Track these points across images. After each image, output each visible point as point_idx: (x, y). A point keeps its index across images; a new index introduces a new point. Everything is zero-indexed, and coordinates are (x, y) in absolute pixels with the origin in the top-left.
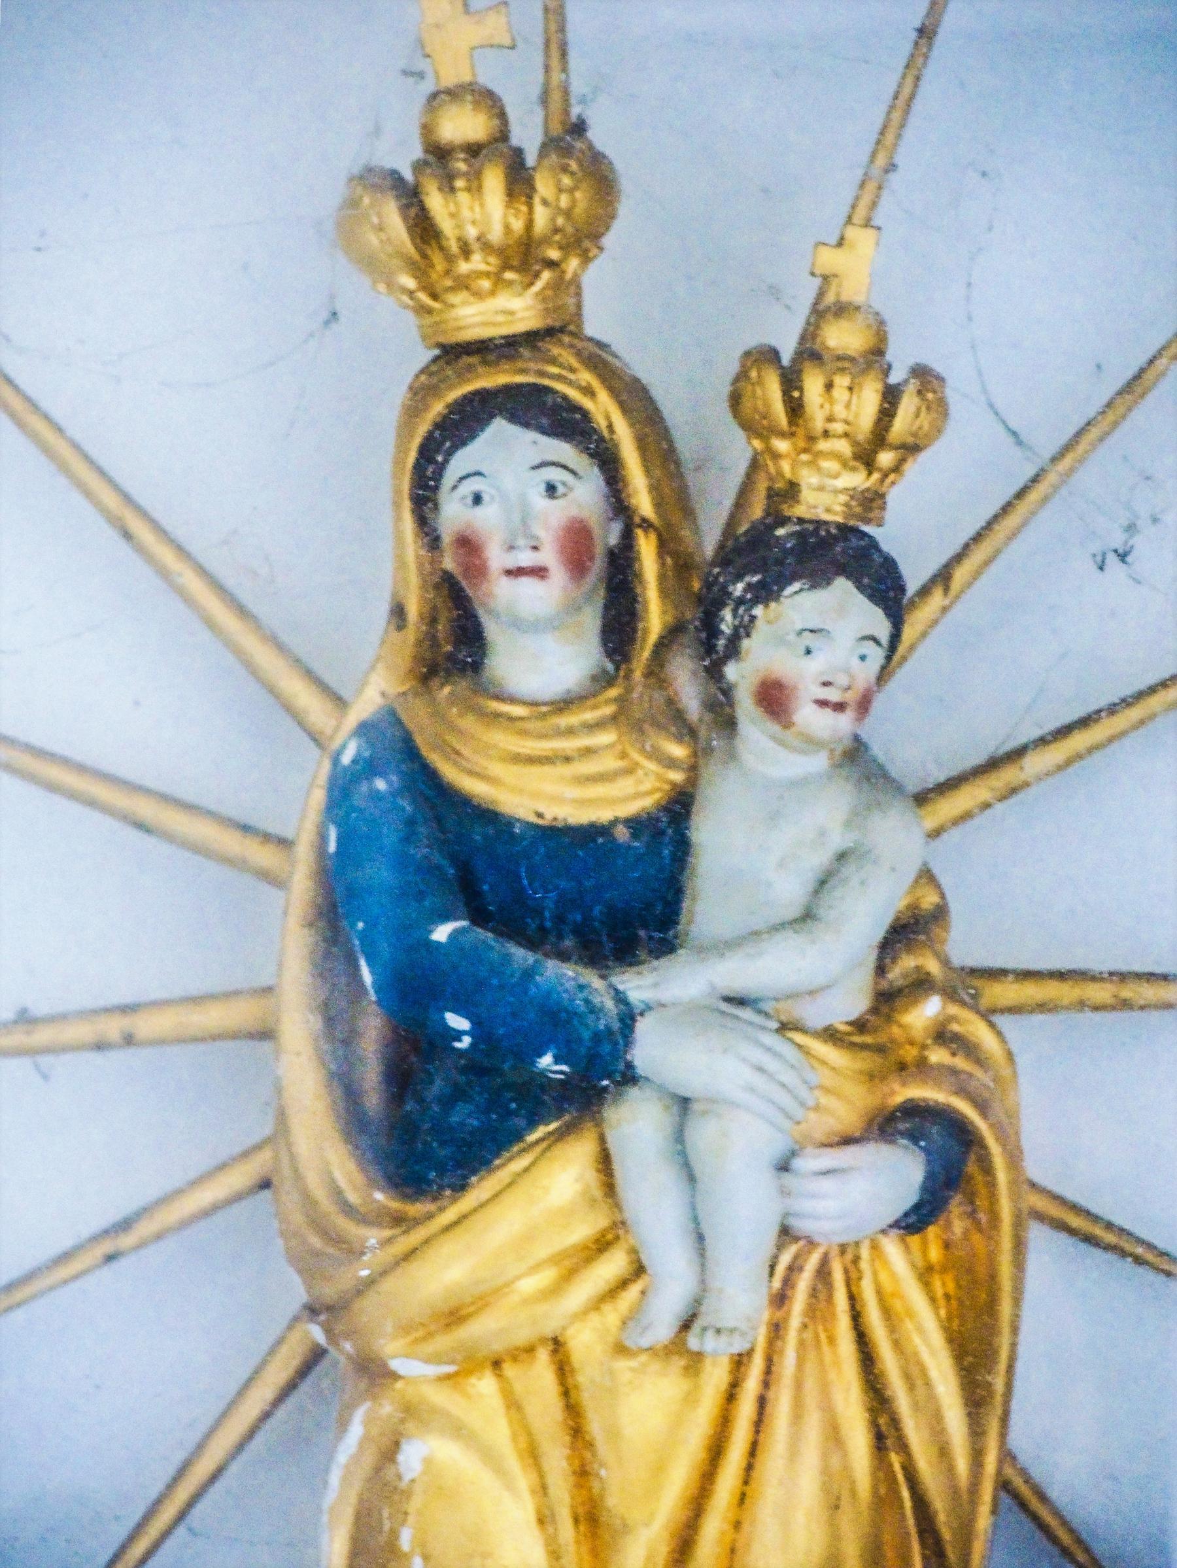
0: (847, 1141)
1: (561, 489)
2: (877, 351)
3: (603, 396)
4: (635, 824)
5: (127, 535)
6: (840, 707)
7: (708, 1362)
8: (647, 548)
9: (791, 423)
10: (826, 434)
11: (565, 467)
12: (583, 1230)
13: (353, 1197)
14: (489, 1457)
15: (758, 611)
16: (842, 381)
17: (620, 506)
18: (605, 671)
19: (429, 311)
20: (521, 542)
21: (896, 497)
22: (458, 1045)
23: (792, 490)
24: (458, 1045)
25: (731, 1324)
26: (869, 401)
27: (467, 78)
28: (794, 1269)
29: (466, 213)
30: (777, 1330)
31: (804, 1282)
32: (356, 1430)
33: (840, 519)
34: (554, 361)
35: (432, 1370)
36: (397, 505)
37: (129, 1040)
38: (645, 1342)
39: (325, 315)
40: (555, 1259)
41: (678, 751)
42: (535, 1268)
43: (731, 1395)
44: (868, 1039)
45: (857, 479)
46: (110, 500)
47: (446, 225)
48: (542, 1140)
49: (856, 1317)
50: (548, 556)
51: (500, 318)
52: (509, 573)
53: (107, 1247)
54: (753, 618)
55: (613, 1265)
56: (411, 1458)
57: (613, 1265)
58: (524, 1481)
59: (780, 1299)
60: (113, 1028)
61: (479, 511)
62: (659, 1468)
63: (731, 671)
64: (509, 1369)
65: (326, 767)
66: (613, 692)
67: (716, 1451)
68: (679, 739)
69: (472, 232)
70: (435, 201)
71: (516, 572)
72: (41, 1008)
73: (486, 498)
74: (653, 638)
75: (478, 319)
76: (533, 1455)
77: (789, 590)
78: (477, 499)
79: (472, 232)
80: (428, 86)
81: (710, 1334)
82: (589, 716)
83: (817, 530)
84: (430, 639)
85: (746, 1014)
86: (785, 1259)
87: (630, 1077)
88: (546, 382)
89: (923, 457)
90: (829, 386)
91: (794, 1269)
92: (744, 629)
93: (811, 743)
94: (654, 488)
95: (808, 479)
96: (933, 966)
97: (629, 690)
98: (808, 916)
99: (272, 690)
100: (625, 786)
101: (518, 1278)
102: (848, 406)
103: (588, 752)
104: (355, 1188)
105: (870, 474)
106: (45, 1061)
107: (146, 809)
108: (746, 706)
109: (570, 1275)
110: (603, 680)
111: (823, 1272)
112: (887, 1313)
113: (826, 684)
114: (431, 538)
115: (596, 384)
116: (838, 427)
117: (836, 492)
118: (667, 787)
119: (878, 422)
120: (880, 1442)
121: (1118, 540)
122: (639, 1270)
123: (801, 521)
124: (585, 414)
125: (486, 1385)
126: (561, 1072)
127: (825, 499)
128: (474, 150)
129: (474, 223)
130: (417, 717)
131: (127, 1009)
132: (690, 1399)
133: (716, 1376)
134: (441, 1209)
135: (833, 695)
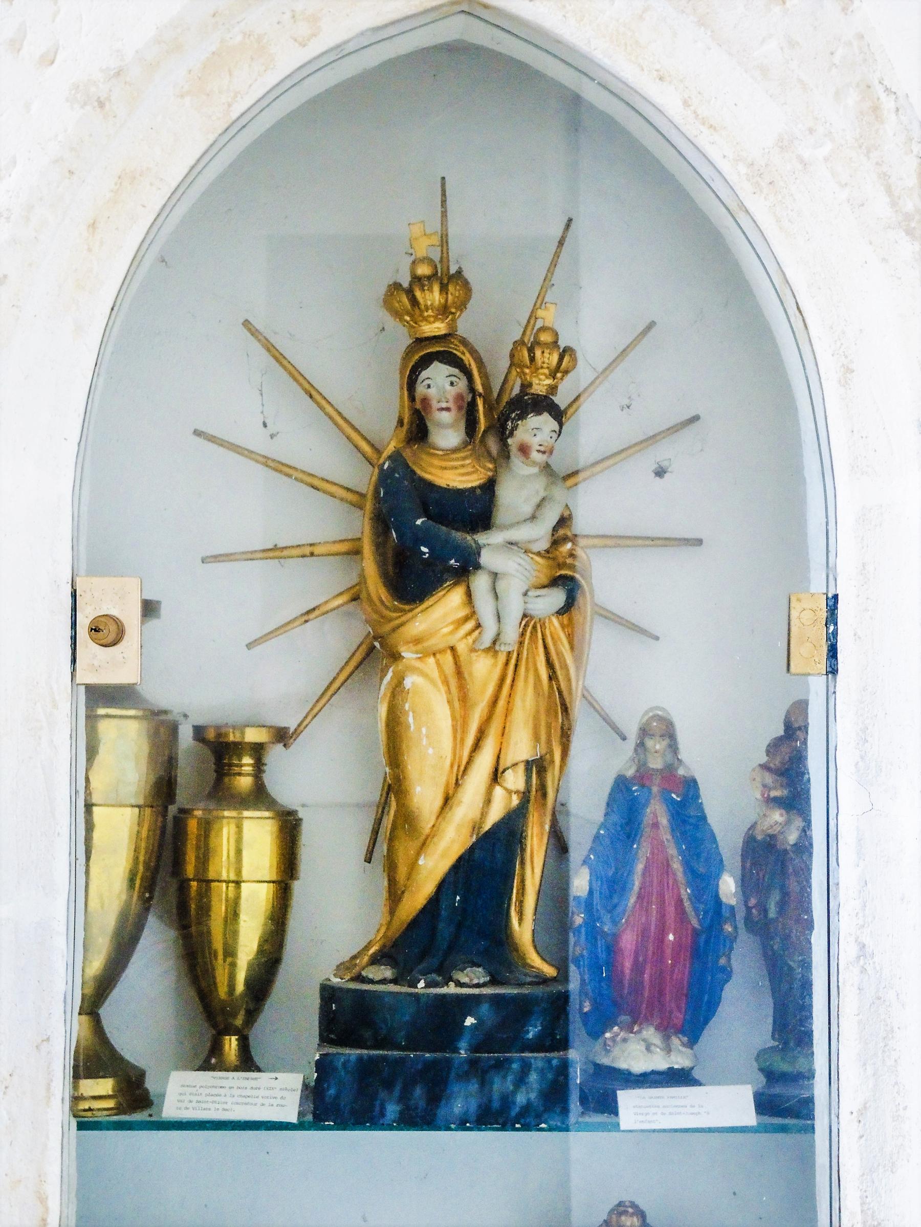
0: (544, 587)
1: (455, 384)
2: (555, 343)
3: (467, 355)
4: (480, 487)
5: (311, 396)
6: (544, 452)
7: (500, 653)
8: (480, 403)
9: (531, 364)
10: (542, 367)
11: (455, 376)
12: (462, 613)
13: (388, 604)
14: (432, 681)
15: (519, 422)
16: (547, 351)
17: (472, 389)
18: (467, 441)
19: (414, 327)
20: (443, 399)
21: (561, 388)
22: (424, 557)
23: (530, 385)
24: (424, 557)
25: (509, 642)
26: (555, 358)
27: (425, 255)
28: (526, 626)
29: (427, 297)
30: (521, 643)
31: (529, 629)
32: (390, 674)
33: (545, 394)
34: (452, 343)
35: (415, 656)
36: (402, 388)
37: (312, 554)
38: (482, 647)
39: (381, 328)
40: (452, 623)
41: (491, 466)
42: (447, 626)
43: (507, 663)
44: (551, 556)
45: (549, 382)
46: (307, 386)
47: (421, 300)
48: (449, 586)
49: (544, 640)
50: (451, 405)
51: (437, 330)
52: (438, 410)
53: (306, 618)
54: (518, 425)
55: (470, 625)
56: (408, 682)
57: (470, 625)
58: (443, 689)
59: (523, 635)
60: (307, 550)
61: (429, 390)
62: (485, 685)
63: (510, 441)
64: (438, 656)
65: (377, 471)
66: (470, 447)
67: (502, 680)
68: (490, 462)
69: (429, 303)
70: (418, 294)
71: (442, 409)
72: (280, 545)
73: (432, 386)
74: (482, 430)
75: (429, 330)
76: (446, 682)
77: (529, 416)
78: (429, 386)
79: (429, 303)
80: (413, 258)
81: (502, 646)
82: (462, 455)
83: (538, 397)
84: (409, 431)
85: (512, 547)
86: (524, 623)
87: (478, 567)
88: (451, 350)
89: (570, 375)
90: (543, 352)
91: (526, 626)
92: (515, 428)
93: (534, 463)
94: (483, 385)
95: (535, 381)
96: (569, 534)
97: (474, 447)
98: (533, 517)
99: (356, 447)
100: (474, 477)
101: (442, 628)
102: (549, 359)
103: (463, 466)
104: (389, 601)
105: (554, 379)
106: (282, 561)
107: (316, 482)
108: (514, 450)
109: (456, 629)
110: (465, 444)
111: (534, 627)
112: (553, 638)
113: (540, 445)
114: (412, 398)
115: (465, 351)
116: (545, 365)
117: (543, 385)
118: (487, 477)
119: (558, 363)
120: (550, 678)
121: (626, 402)
122: (478, 626)
123: (534, 394)
124: (462, 360)
125: (431, 660)
126: (457, 565)
127: (540, 388)
128: (429, 278)
129: (430, 300)
130: (407, 454)
131: (311, 545)
132: (495, 665)
133: (502, 658)
134: (417, 607)
135: (542, 449)
